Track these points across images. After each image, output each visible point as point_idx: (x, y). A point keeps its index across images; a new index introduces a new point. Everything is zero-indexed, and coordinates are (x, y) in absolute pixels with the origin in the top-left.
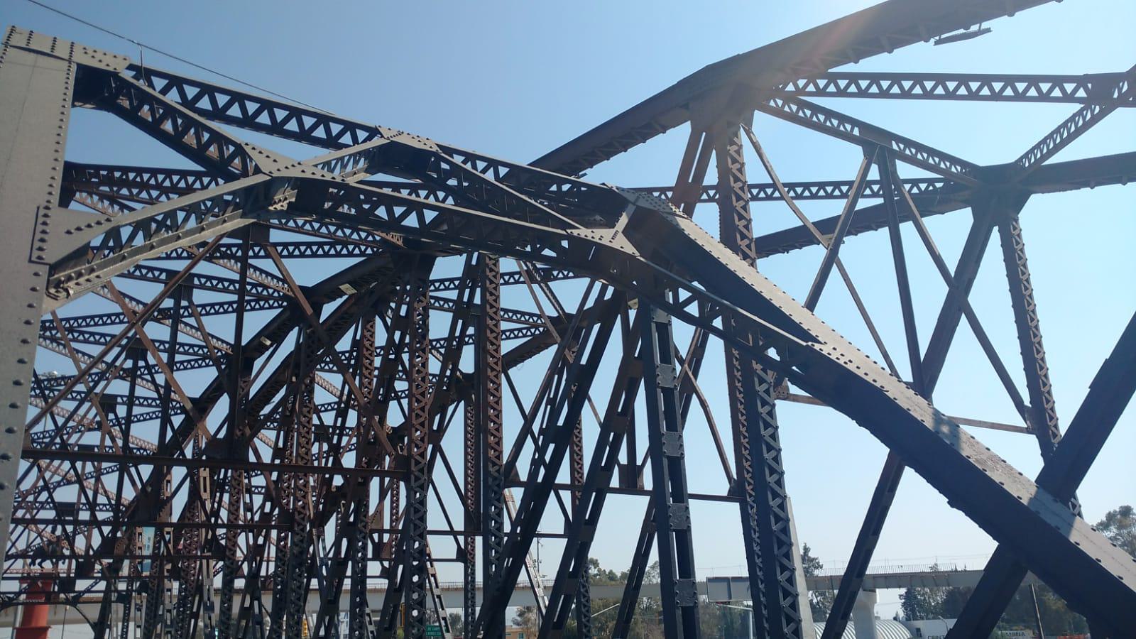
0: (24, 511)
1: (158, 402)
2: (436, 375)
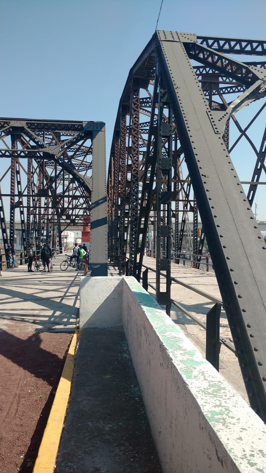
1: (221, 92)
2: (213, 95)
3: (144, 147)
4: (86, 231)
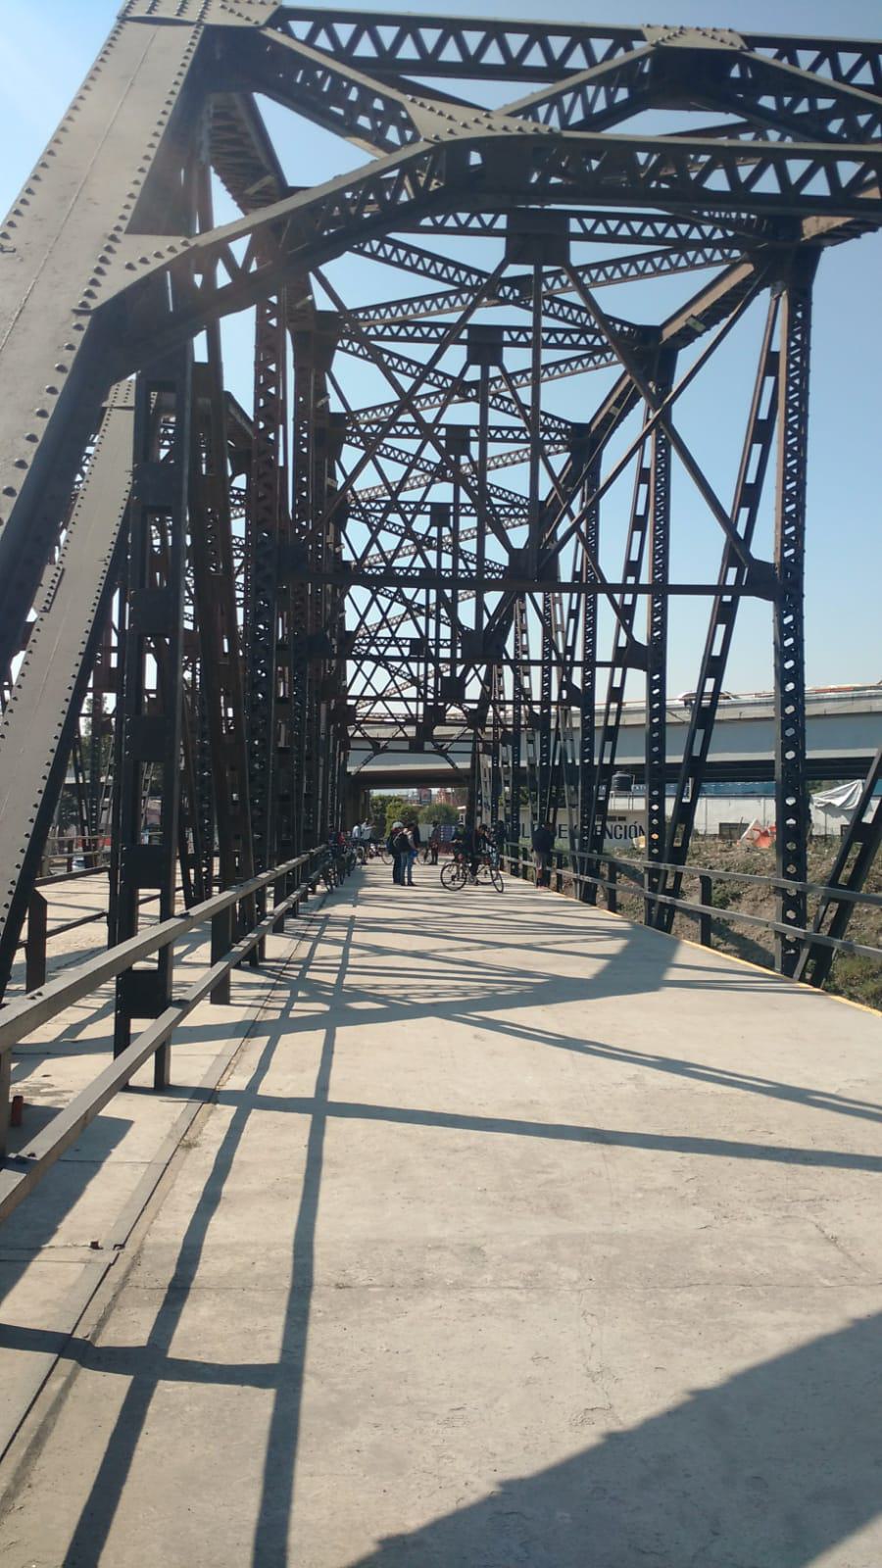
0: (413, 421)
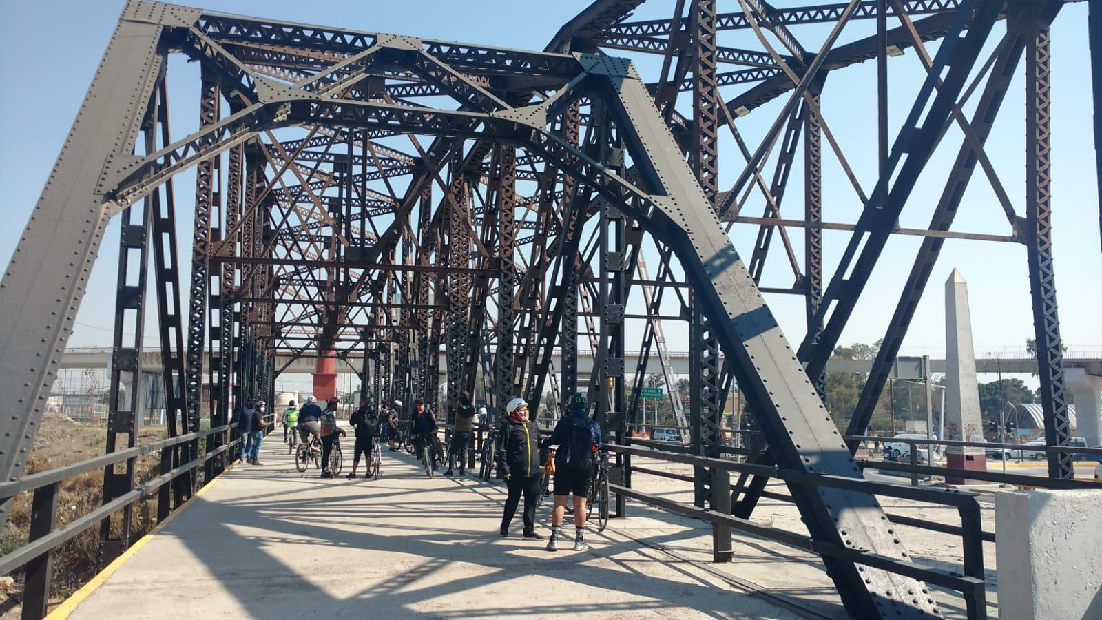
3: (378, 178)
4: (325, 373)
